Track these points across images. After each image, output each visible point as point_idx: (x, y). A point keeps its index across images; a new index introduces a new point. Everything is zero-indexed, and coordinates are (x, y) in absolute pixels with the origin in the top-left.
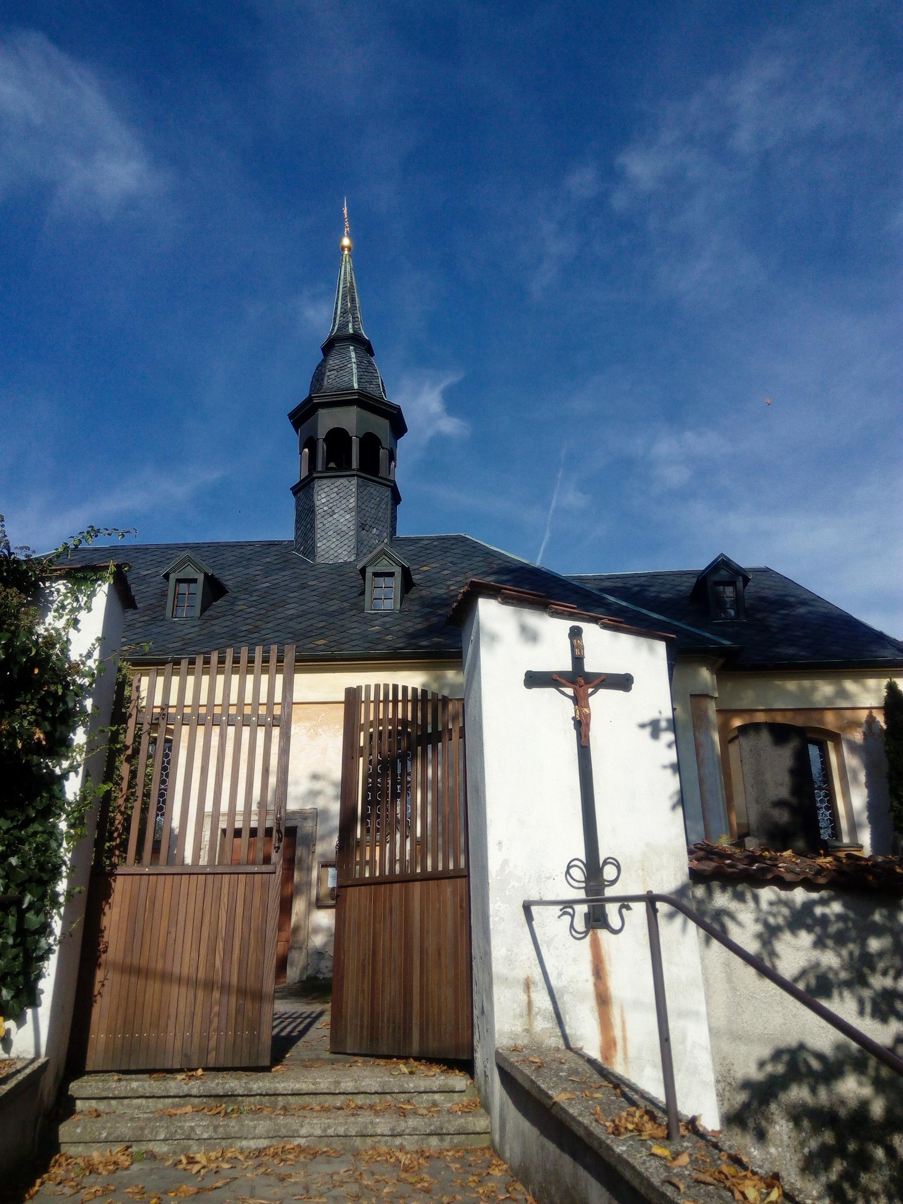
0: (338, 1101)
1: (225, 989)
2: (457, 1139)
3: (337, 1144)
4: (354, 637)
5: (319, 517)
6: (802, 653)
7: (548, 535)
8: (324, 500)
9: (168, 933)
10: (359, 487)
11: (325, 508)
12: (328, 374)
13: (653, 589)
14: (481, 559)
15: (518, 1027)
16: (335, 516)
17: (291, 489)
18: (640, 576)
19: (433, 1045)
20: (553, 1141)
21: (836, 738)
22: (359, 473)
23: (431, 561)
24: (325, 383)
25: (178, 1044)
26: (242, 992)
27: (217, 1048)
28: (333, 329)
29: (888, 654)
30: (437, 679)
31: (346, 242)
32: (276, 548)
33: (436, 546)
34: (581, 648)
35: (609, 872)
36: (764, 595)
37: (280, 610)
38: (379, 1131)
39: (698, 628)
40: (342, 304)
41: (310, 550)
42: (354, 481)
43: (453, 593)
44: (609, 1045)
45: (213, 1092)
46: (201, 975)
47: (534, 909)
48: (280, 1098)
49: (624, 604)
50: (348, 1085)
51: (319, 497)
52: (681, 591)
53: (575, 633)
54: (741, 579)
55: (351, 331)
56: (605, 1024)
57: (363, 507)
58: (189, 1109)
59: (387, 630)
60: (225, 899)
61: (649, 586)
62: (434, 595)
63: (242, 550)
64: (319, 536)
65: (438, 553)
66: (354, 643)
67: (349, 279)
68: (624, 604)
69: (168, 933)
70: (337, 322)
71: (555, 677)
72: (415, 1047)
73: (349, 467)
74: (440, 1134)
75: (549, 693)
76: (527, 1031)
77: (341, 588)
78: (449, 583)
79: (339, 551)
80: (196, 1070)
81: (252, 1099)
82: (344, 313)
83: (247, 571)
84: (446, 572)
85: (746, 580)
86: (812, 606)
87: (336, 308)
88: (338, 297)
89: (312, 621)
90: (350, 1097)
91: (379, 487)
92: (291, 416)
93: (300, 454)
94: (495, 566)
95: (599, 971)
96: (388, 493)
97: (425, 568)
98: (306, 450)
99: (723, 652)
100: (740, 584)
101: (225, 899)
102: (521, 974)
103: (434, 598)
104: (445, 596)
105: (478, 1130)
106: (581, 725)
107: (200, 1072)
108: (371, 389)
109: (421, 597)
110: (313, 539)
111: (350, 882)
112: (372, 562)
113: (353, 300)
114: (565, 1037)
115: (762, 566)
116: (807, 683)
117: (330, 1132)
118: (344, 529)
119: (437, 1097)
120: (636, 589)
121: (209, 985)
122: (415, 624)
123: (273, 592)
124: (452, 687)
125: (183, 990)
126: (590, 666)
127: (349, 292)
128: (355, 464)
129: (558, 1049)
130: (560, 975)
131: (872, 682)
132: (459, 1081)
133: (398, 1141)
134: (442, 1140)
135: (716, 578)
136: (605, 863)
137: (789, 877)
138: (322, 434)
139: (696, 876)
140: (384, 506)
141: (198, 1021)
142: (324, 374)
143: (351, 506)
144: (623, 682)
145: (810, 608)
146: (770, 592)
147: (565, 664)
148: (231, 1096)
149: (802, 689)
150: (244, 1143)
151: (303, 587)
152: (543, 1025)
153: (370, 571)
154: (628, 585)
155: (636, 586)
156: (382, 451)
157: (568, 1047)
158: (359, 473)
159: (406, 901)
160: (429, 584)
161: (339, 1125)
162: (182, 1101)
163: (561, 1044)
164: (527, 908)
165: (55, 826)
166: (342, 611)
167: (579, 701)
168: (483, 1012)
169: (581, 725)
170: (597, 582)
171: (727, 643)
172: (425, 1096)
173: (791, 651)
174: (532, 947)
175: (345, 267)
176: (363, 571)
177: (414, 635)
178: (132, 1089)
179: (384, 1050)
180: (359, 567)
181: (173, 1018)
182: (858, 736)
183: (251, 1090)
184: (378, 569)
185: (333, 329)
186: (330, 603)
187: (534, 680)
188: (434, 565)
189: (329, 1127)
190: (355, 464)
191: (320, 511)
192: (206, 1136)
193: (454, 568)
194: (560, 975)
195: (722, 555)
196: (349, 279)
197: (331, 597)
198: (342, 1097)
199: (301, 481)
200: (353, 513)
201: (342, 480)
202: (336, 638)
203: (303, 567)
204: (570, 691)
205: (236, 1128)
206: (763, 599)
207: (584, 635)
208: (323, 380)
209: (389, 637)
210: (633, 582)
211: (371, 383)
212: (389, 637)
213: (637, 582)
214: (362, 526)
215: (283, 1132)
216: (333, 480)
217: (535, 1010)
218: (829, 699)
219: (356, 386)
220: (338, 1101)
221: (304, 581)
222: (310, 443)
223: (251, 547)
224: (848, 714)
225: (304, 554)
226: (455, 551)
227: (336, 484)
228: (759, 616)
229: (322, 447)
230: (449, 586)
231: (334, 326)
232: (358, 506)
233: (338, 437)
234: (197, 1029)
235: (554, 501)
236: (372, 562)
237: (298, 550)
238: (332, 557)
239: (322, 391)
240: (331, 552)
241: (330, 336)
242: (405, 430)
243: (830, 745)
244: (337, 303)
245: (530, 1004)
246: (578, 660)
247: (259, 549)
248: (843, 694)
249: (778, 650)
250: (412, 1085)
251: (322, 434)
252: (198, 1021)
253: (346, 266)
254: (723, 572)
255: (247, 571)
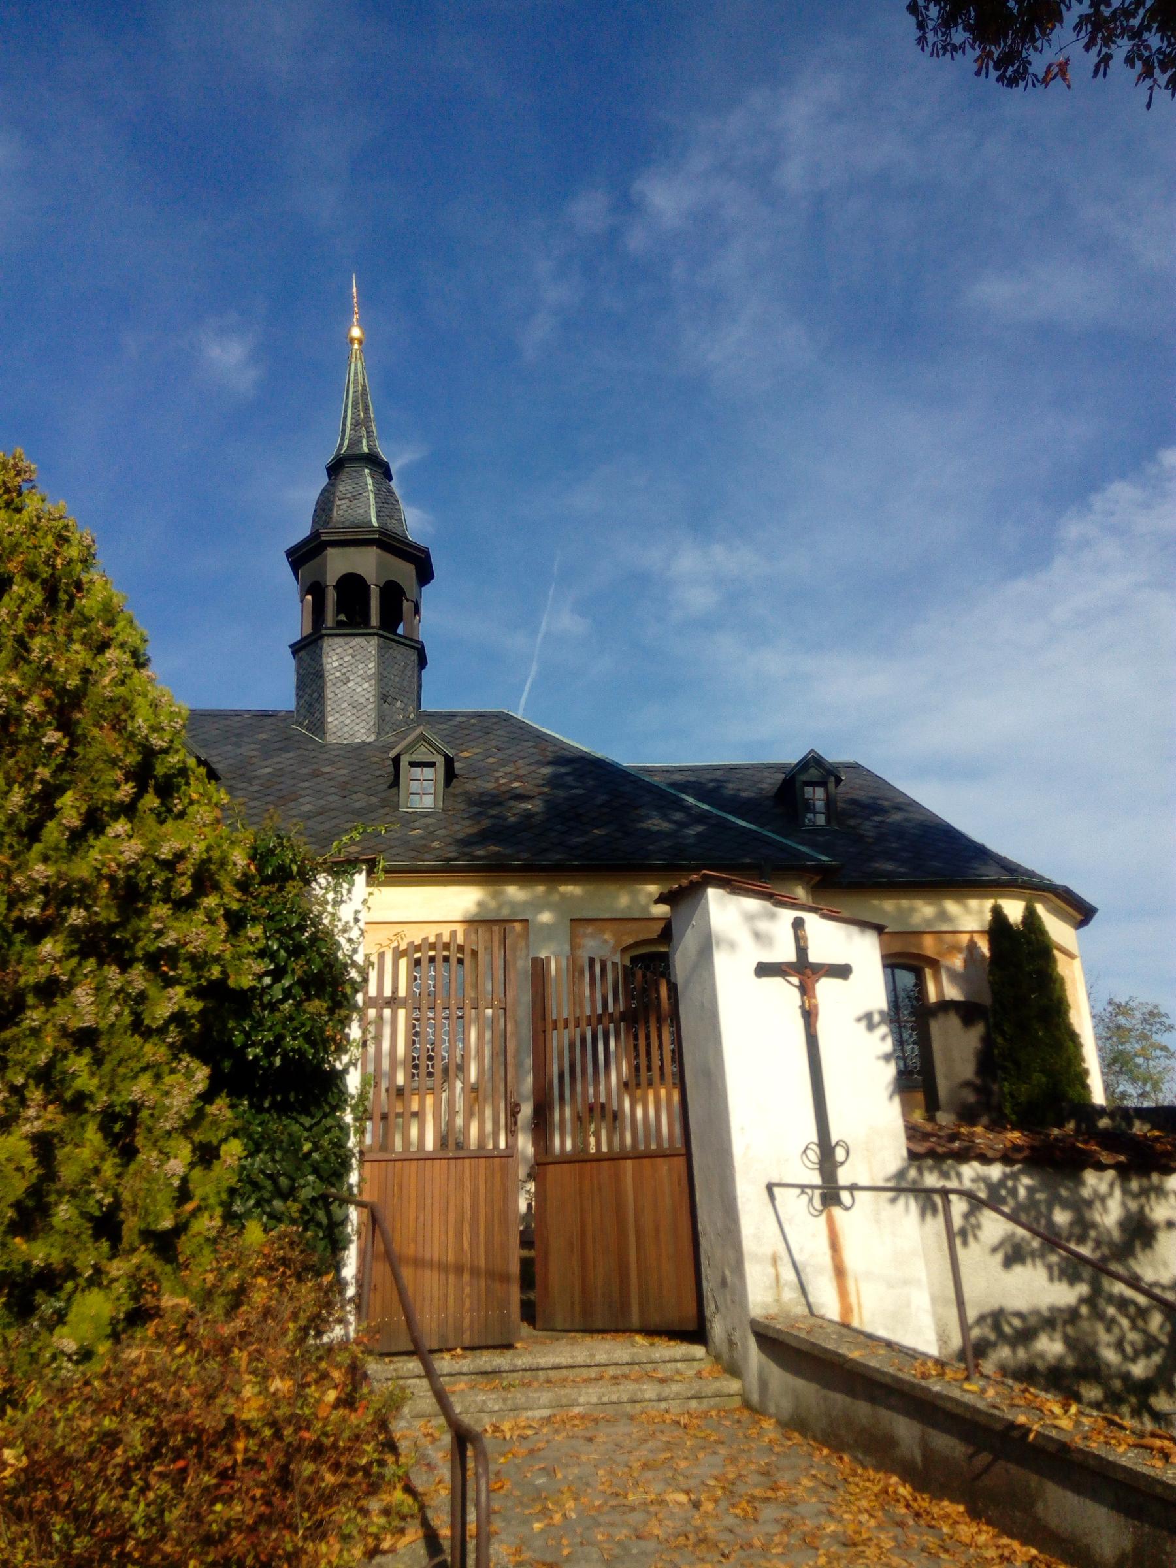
0: (593, 1373)
1: (475, 1272)
2: (713, 1401)
3: (610, 1410)
4: (392, 843)
5: (329, 684)
6: (902, 870)
7: (534, 668)
8: (335, 664)
9: (417, 1217)
10: (380, 648)
11: (338, 674)
12: (338, 503)
13: (730, 786)
14: (531, 744)
15: (769, 1298)
16: (350, 685)
17: (291, 646)
18: (716, 768)
19: (654, 1320)
20: (841, 1391)
21: (934, 964)
22: (381, 632)
23: (472, 744)
24: (335, 514)
25: (434, 1325)
26: (491, 1275)
27: (471, 1328)
28: (341, 445)
29: (992, 872)
30: (495, 896)
31: (356, 332)
32: (269, 720)
33: (473, 725)
34: (805, 939)
35: (840, 1154)
36: (855, 797)
37: (291, 805)
38: (647, 1396)
39: (785, 836)
40: (353, 413)
41: (318, 726)
42: (374, 641)
43: (503, 788)
44: (846, 1309)
45: (482, 1370)
46: (451, 1258)
47: (776, 1190)
48: (541, 1373)
49: (706, 807)
50: (602, 1357)
51: (329, 660)
52: (762, 789)
53: (798, 924)
54: (833, 779)
55: (366, 450)
56: (843, 1292)
57: (385, 673)
58: (462, 1386)
59: (431, 835)
60: (467, 1183)
61: (726, 782)
62: (481, 791)
63: (228, 722)
64: (329, 708)
65: (478, 734)
66: (394, 851)
67: (360, 381)
68: (706, 807)
69: (417, 1217)
70: (347, 436)
71: (784, 968)
72: (635, 1321)
73: (366, 623)
74: (698, 1397)
75: (777, 982)
76: (777, 1301)
77: (365, 777)
78: (499, 774)
79: (356, 729)
80: (455, 1349)
81: (515, 1374)
82: (356, 424)
83: (239, 751)
84: (491, 760)
85: (838, 781)
86: (906, 811)
87: (345, 418)
88: (347, 406)
89: (337, 821)
90: (603, 1368)
91: (403, 649)
92: (290, 553)
93: (302, 602)
94: (548, 753)
95: (835, 1246)
96: (414, 657)
97: (466, 754)
98: (309, 597)
99: (821, 869)
100: (831, 785)
101: (467, 1183)
102: (767, 1250)
103: (482, 795)
104: (495, 792)
105: (732, 1392)
106: (809, 1016)
107: (459, 1351)
108: (392, 525)
109: (466, 793)
110: (322, 712)
111: (551, 1160)
112: (409, 748)
113: (366, 408)
114: (809, 1305)
115: (851, 761)
116: (905, 903)
117: (605, 1399)
118: (362, 700)
119: (679, 1365)
120: (711, 785)
121: (459, 1269)
122: (464, 829)
123: (279, 780)
124: (513, 905)
125: (436, 1275)
126: (814, 957)
127: (362, 398)
128: (374, 620)
129: (805, 1317)
130: (801, 1250)
131: (973, 903)
132: (698, 1351)
133: (663, 1405)
134: (699, 1403)
135: (804, 777)
136: (837, 1144)
137: (990, 1154)
138: (331, 579)
139: (913, 1156)
140: (409, 673)
141: (451, 1302)
142: (333, 502)
143: (370, 672)
144: (842, 971)
145: (906, 815)
146: (863, 793)
147: (790, 956)
148: (497, 1372)
149: (900, 910)
150: (530, 1413)
151: (316, 774)
152: (790, 1295)
153: (405, 760)
154: (703, 781)
155: (712, 781)
156: (405, 604)
157: (812, 1314)
158: (381, 632)
159: (617, 1178)
160: (473, 775)
161: (613, 1394)
162: (453, 1379)
163: (806, 1311)
164: (770, 1188)
165: (341, 1118)
166: (371, 809)
167: (805, 990)
168: (724, 1283)
169: (809, 1016)
170: (667, 775)
171: (825, 858)
172: (669, 1365)
173: (889, 866)
174: (776, 1225)
175: (356, 366)
176: (396, 761)
177: (465, 842)
178: (409, 1370)
179: (599, 1325)
180: (392, 754)
181: (427, 1303)
182: (958, 962)
183: (515, 1366)
184: (416, 758)
185: (341, 445)
186: (354, 797)
187: (764, 970)
188: (476, 750)
189: (604, 1395)
190: (374, 620)
191: (331, 677)
192: (496, 1408)
193: (500, 755)
194: (801, 1250)
195: (812, 751)
196: (360, 381)
197: (355, 789)
198: (596, 1369)
199: (303, 639)
200: (373, 682)
201: (358, 640)
202: (372, 844)
203: (310, 747)
204: (795, 980)
205: (523, 1400)
206: (854, 802)
207: (807, 926)
208: (331, 510)
209: (436, 844)
210: (709, 777)
211: (391, 518)
212: (436, 844)
213: (714, 777)
214: (384, 698)
215: (564, 1401)
216: (347, 639)
217: (782, 1281)
218: (928, 922)
219: (374, 522)
220: (593, 1373)
221: (315, 767)
222: (315, 590)
223: (238, 718)
224: (948, 937)
225: (308, 730)
226: (499, 733)
227: (351, 644)
228: (852, 822)
229: (331, 597)
230: (497, 779)
231: (343, 440)
232: (379, 673)
233: (352, 585)
234: (451, 1310)
235: (543, 624)
236: (409, 748)
237: (300, 724)
238: (346, 735)
239: (331, 525)
240: (346, 729)
241: (337, 455)
242: (432, 576)
243: (928, 972)
244: (346, 411)
245: (777, 1277)
246: (802, 951)
247: (249, 721)
248: (943, 916)
249: (877, 865)
250: (658, 1355)
251: (331, 579)
252: (451, 1302)
253: (357, 366)
254: (813, 771)
255: (239, 751)
